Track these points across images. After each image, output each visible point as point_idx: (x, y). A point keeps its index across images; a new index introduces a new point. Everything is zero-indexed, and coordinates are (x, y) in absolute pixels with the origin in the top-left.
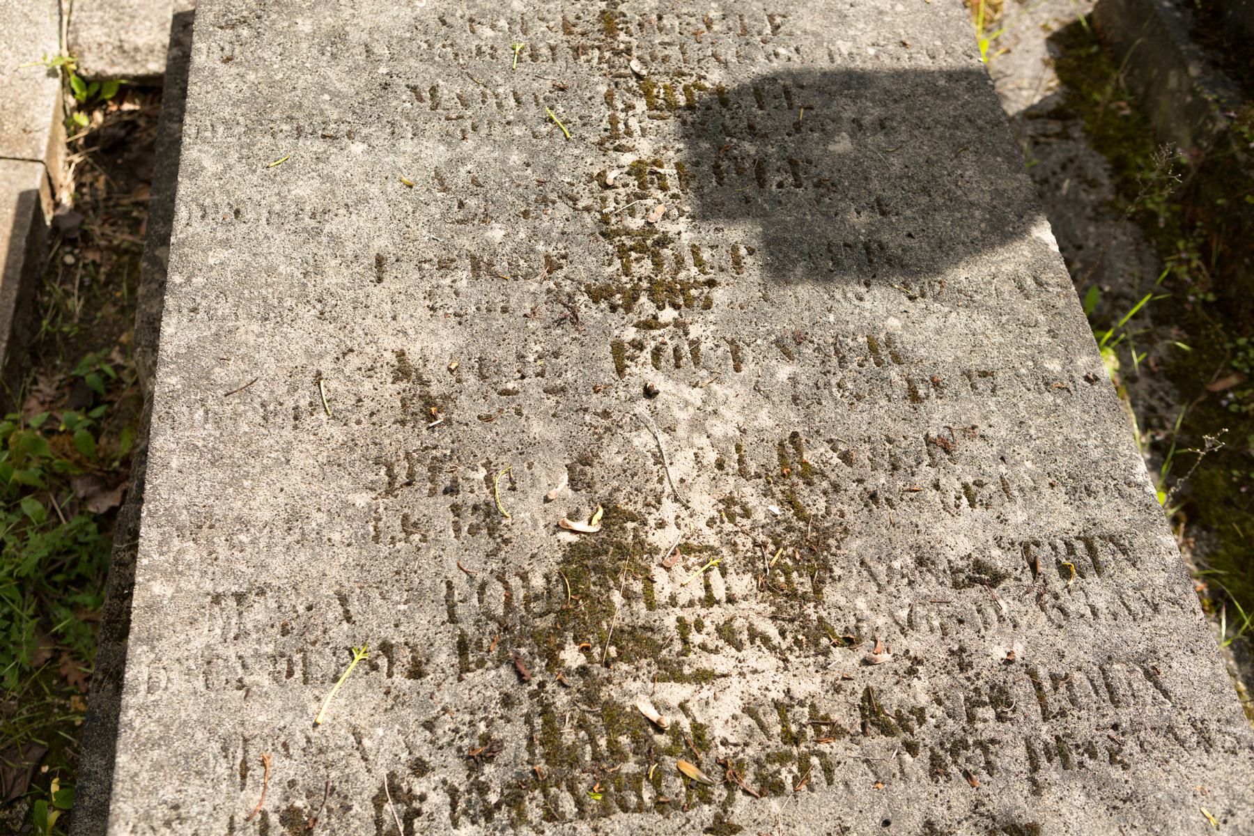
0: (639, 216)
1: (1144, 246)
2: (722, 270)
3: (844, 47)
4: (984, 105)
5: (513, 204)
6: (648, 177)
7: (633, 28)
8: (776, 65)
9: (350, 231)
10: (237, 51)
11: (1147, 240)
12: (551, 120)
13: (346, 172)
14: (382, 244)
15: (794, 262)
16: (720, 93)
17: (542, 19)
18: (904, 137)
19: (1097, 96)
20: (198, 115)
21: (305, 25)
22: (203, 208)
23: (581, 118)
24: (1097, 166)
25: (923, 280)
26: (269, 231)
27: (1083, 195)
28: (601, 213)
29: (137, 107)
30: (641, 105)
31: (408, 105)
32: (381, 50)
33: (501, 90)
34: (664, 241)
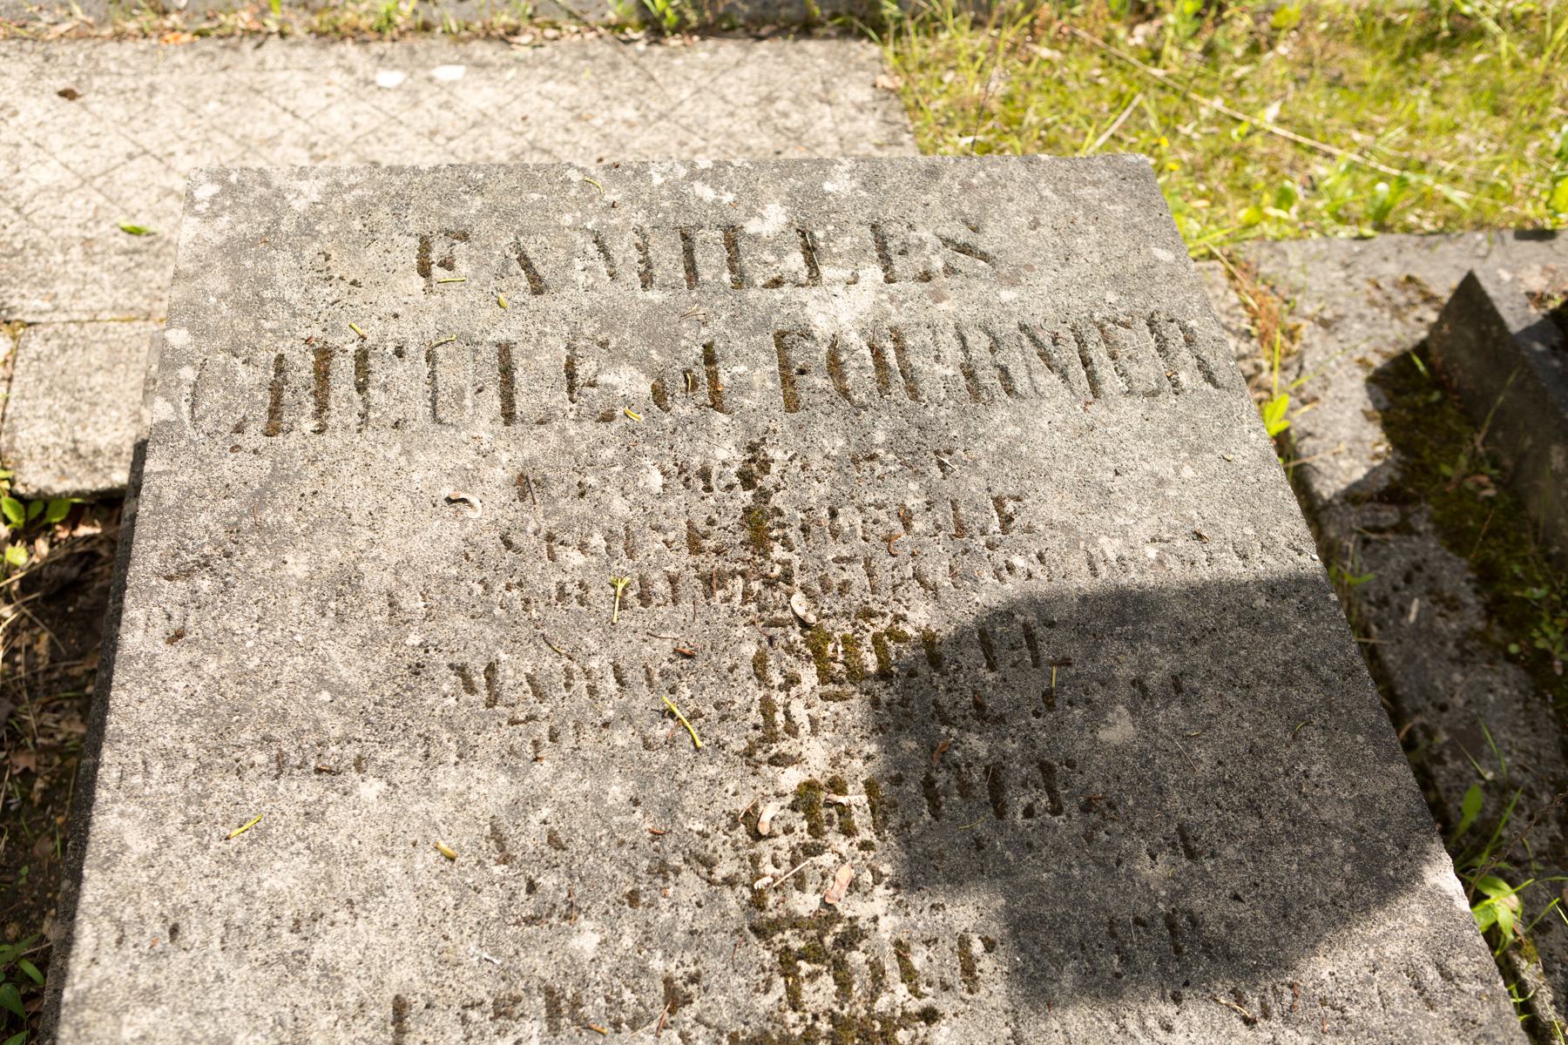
0: (811, 887)
1: (1535, 704)
2: (946, 987)
3: (1110, 547)
4: (1327, 639)
5: (613, 880)
6: (824, 812)
7: (793, 534)
8: (1013, 587)
9: (355, 955)
10: (191, 622)
11: (1538, 693)
12: (672, 715)
13: (351, 837)
14: (405, 976)
15: (1059, 962)
16: (928, 640)
17: (657, 528)
18: (1211, 707)
19: (1446, 470)
20: (122, 746)
21: (297, 566)
22: (120, 926)
23: (717, 706)
24: (1455, 576)
25: (1263, 982)
26: (223, 963)
27: (1440, 622)
28: (753, 891)
29: (98, 531)
30: (809, 676)
31: (451, 701)
32: (412, 603)
33: (594, 664)
34: (852, 937)
